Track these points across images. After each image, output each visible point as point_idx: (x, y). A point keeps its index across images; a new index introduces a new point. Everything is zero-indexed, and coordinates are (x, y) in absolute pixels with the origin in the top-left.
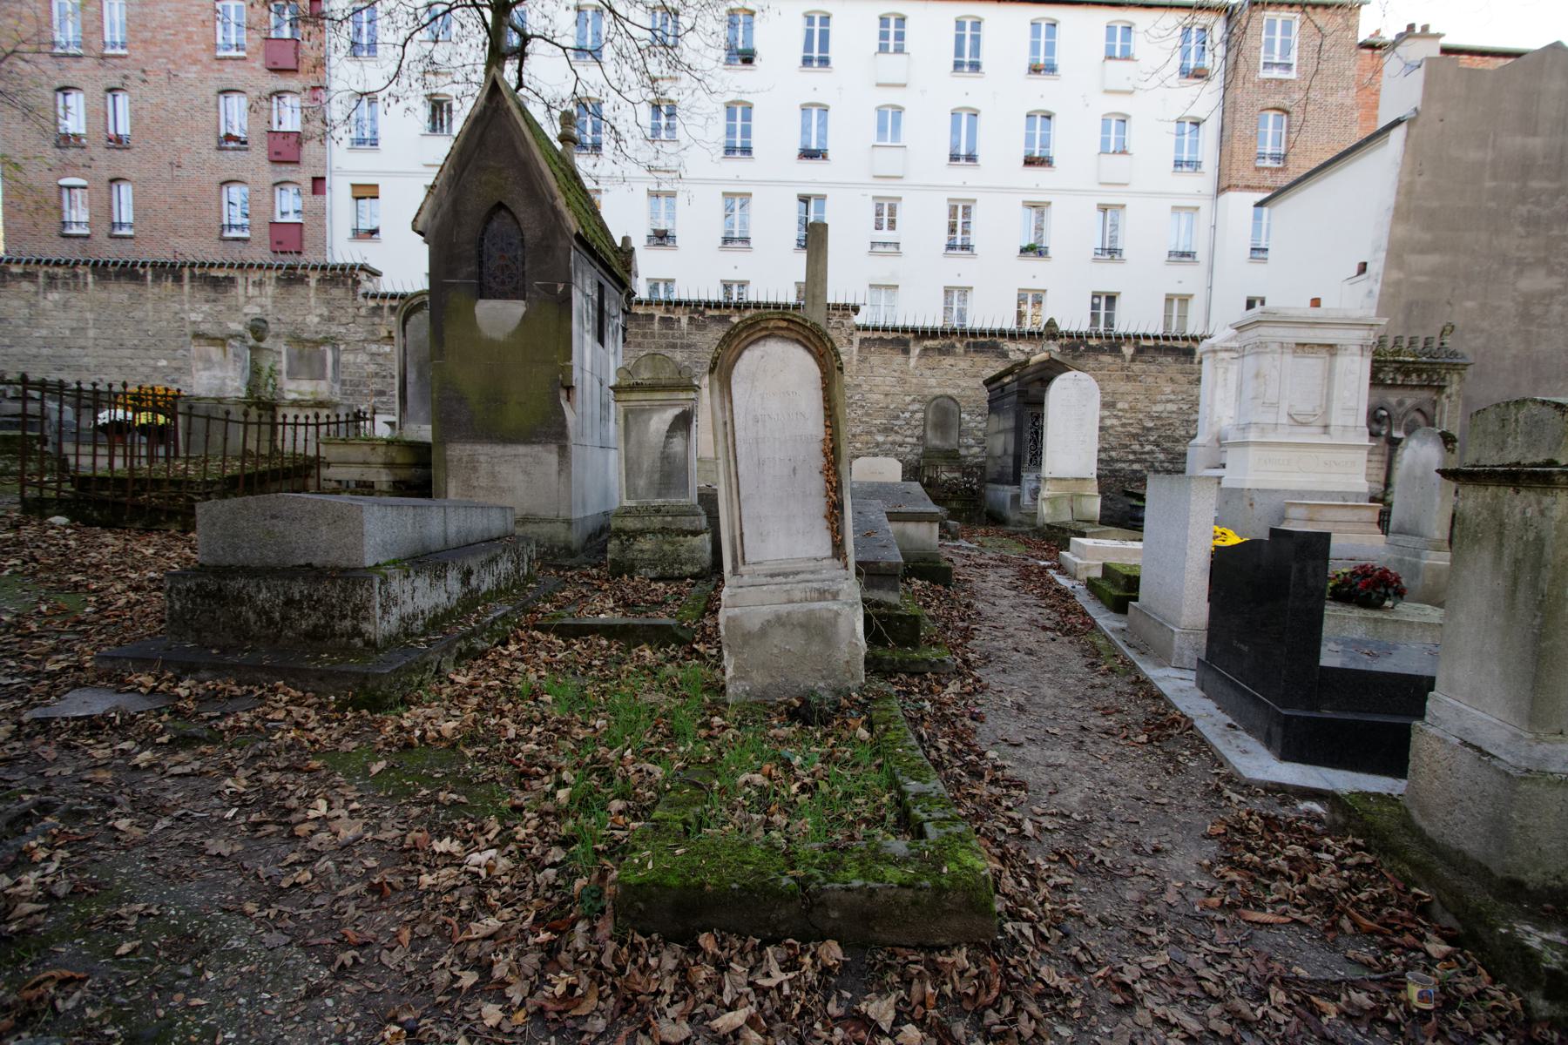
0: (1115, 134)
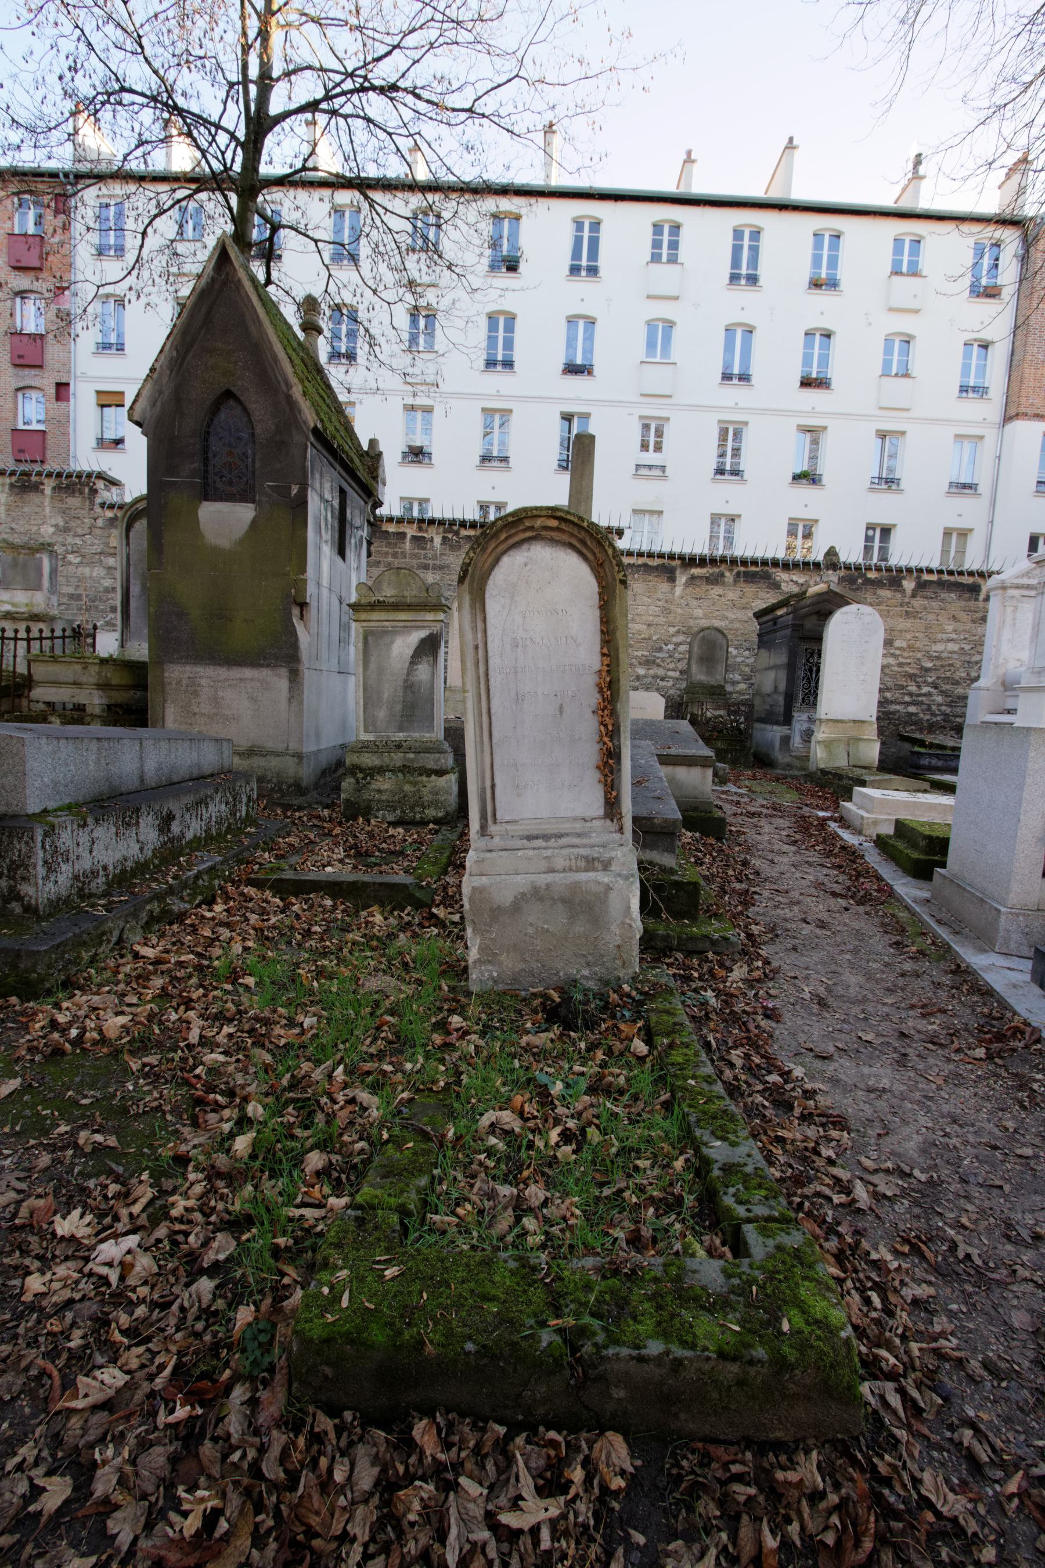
0: (899, 356)
